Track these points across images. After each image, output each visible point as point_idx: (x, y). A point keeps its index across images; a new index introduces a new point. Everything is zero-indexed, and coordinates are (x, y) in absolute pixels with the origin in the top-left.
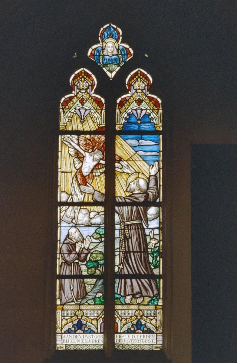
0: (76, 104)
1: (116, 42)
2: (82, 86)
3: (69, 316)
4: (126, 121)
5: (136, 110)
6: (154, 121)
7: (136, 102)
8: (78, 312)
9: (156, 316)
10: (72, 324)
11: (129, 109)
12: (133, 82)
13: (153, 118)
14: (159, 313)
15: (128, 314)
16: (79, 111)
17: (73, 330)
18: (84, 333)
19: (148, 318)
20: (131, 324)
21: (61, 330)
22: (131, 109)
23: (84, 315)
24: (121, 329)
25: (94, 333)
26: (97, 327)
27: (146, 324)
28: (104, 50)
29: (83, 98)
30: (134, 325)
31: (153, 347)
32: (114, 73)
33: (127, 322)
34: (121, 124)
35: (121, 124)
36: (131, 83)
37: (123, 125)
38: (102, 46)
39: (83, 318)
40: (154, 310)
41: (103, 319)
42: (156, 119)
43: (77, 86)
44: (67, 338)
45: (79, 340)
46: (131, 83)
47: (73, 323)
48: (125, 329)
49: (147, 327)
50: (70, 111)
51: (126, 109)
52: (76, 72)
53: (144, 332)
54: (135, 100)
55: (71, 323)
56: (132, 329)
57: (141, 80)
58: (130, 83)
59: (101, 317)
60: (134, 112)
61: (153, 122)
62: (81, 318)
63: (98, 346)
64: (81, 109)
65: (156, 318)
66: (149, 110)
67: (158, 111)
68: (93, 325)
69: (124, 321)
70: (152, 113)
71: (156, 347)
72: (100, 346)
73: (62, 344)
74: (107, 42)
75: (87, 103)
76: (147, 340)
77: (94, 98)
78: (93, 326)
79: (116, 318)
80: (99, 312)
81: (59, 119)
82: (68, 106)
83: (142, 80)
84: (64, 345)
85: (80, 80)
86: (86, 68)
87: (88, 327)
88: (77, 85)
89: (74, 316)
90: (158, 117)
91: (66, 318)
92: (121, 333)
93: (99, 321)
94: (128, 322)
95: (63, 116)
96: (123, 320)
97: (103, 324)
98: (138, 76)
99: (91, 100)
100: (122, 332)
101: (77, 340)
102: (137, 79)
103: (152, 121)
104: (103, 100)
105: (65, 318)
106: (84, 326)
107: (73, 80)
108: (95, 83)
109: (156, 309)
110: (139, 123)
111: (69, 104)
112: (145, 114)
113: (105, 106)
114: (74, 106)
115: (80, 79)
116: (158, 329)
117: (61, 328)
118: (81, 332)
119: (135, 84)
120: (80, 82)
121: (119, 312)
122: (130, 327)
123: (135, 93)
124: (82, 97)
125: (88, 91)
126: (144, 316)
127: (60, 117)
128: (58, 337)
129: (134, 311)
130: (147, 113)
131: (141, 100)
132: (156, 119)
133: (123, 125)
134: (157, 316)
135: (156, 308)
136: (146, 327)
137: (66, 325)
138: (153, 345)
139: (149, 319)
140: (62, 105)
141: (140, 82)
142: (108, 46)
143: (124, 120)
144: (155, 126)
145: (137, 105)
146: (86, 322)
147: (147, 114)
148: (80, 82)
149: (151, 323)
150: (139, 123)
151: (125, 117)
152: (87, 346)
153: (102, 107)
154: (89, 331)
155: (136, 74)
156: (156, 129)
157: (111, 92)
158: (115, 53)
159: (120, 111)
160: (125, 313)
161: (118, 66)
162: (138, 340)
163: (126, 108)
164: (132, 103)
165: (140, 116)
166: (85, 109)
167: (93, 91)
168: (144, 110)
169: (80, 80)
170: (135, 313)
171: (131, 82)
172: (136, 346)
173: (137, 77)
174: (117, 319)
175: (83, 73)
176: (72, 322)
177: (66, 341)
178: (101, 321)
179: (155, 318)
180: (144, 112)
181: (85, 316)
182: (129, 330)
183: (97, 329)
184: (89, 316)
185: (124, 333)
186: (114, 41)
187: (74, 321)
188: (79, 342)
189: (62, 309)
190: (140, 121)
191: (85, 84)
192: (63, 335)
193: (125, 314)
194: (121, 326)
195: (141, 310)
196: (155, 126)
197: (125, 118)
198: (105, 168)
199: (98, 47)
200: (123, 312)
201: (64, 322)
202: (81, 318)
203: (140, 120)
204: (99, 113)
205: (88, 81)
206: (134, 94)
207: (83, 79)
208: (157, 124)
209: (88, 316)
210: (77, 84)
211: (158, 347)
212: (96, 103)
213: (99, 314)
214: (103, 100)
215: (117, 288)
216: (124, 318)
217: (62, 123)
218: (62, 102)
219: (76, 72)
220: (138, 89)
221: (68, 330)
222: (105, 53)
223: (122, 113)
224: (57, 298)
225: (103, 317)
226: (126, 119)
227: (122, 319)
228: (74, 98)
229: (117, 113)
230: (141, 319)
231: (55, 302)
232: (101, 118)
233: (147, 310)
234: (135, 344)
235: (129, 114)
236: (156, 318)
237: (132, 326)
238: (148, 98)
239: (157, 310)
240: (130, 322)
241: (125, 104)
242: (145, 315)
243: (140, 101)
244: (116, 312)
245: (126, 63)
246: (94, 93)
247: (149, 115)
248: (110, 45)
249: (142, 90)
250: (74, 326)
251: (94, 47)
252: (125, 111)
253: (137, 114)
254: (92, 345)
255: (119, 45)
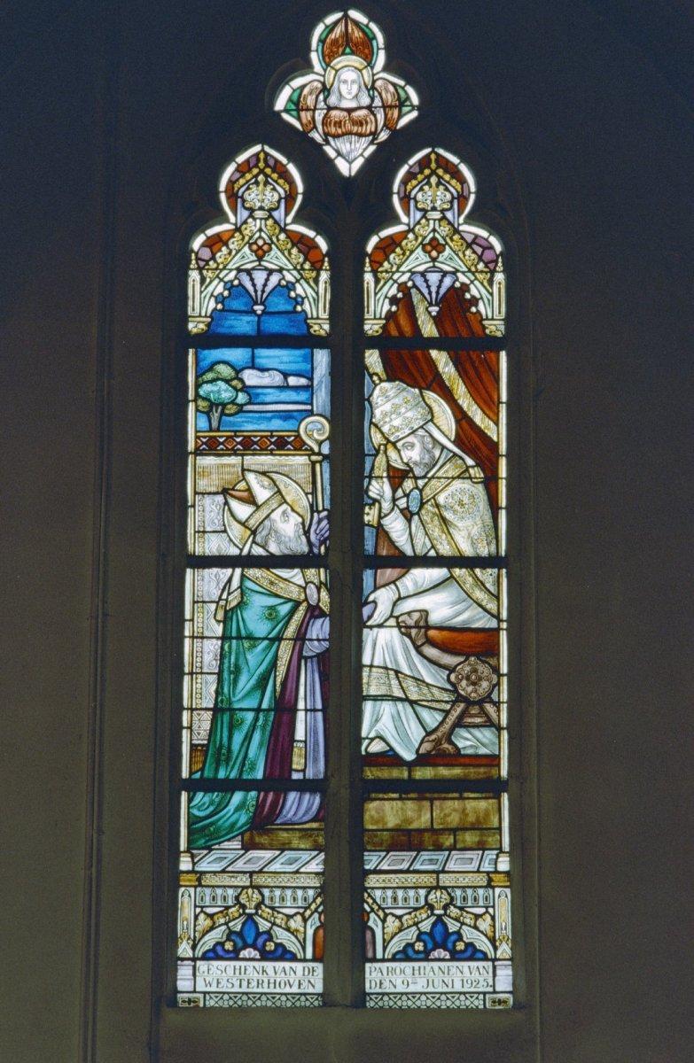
0: (239, 255)
1: (366, 67)
2: (432, 201)
3: (220, 906)
4: (220, 306)
5: (423, 274)
6: (307, 306)
7: (424, 250)
8: (247, 893)
9: (492, 904)
10: (418, 932)
11: (404, 273)
12: (245, 184)
13: (303, 299)
14: (499, 896)
15: (295, 899)
16: (248, 278)
17: (421, 948)
18: (453, 959)
19: (468, 912)
20: (227, 931)
21: (194, 948)
22: (410, 271)
23: (262, 902)
24: (385, 948)
25: (294, 958)
26: (305, 939)
27: (462, 931)
28: (329, 91)
29: (434, 239)
30: (425, 933)
31: (484, 1000)
32: (359, 163)
33: (214, 923)
34: (203, 314)
35: (203, 314)
36: (236, 189)
37: (209, 320)
38: (322, 79)
39: (260, 912)
40: (486, 887)
41: (322, 917)
42: (487, 305)
43: (416, 202)
44: (432, 973)
45: (312, 982)
46: (236, 189)
47: (418, 929)
48: (396, 946)
49: (467, 941)
50: (395, 277)
51: (221, 270)
52: (241, 158)
53: (265, 956)
54: (421, 243)
55: (414, 928)
56: (229, 946)
57: (267, 179)
58: (233, 188)
59: (316, 910)
60: (419, 281)
61: (303, 311)
62: (442, 912)
63: (448, 999)
64: (430, 272)
65: (491, 910)
66: (463, 273)
67: (492, 276)
68: (480, 934)
69: (392, 924)
70: (298, 281)
71: (494, 1002)
72: (472, 997)
73: (195, 992)
74: (337, 67)
75: (272, 253)
76: (302, 981)
77: (469, 238)
78: (481, 935)
79: (368, 914)
80: (311, 893)
81: (363, 308)
82: (389, 263)
83: (269, 180)
84: (201, 996)
85: (253, 180)
86: (272, 146)
87: (465, 939)
88: (415, 198)
89: (234, 906)
90: (317, 293)
91: (210, 911)
92: (383, 960)
93: (309, 923)
94: (406, 926)
95: (201, 292)
96: (390, 919)
97: (321, 932)
98: (429, 167)
99: (456, 243)
100: (386, 957)
101: (441, 981)
102: (428, 177)
103: (299, 308)
104: (323, 245)
105: (204, 909)
106: (453, 938)
107: (405, 182)
108: (469, 190)
109: (492, 884)
110: (259, 312)
111: (392, 256)
112: (279, 284)
113: (503, 262)
114: (233, 261)
115: (424, 179)
116: (497, 944)
117: (194, 940)
118: (256, 955)
119: (247, 192)
120: (426, 188)
121: (378, 894)
122: (274, 939)
123: (250, 220)
124: (431, 235)
125: (277, 214)
126: (455, 907)
127: (366, 296)
128: (184, 971)
129: (422, 892)
130: (283, 283)
131: (439, 244)
132: (487, 305)
133: (209, 320)
134: (493, 907)
135: (490, 880)
136: (270, 939)
137: (396, 934)
138: (485, 994)
139: (469, 915)
140: (371, 261)
141: (265, 185)
142: (343, 77)
143: (212, 305)
144: (308, 321)
145: (255, 258)
146: (270, 925)
147: (283, 287)
148: (426, 188)
149: (288, 929)
150: (259, 312)
151: (215, 294)
152: (472, 997)
153: (492, 266)
154: (468, 953)
155: (424, 163)
156: (485, 333)
157: (347, 215)
158: (365, 101)
159: (201, 274)
160: (225, 897)
161: (372, 143)
162: (260, 982)
163: (221, 267)
164: (412, 252)
165: (263, 291)
166: (441, 271)
167: (461, 220)
168: (450, 272)
169: (253, 180)
170: (426, 897)
171: (409, 187)
172: (293, 998)
173: (427, 172)
174: (372, 915)
175: (262, 161)
176: (416, 924)
177: (208, 980)
178: (314, 922)
179: (487, 912)
180: (274, 279)
181: (266, 906)
182: (410, 952)
183: (304, 948)
184: (279, 907)
185: (394, 959)
186: (356, 61)
187: (234, 920)
188: (313, 986)
189: (197, 883)
190: (262, 307)
191: (442, 197)
192: (198, 963)
193: (225, 900)
194: (384, 940)
195: (445, 888)
196: (308, 321)
197: (216, 298)
198: (186, 450)
199: (310, 82)
200: (389, 893)
201: (203, 922)
202: (253, 911)
203: (262, 303)
204: (308, 283)
205: (450, 184)
206: (419, 223)
207: (261, 178)
208: (490, 317)
209: (277, 905)
210: (245, 191)
211: (500, 1002)
212: (300, 251)
213: (311, 900)
214: (323, 245)
215: (497, 817)
216: (393, 915)
217: (373, 317)
218: (370, 248)
219: (241, 158)
220: (257, 208)
221: (404, 951)
222: (333, 100)
223: (382, 282)
224: (182, 849)
225: (320, 909)
226: (220, 299)
227: (386, 915)
228: (406, 238)
229: (368, 283)
230: (257, 913)
231: (176, 862)
232: (490, 298)
233: (384, 888)
234: (428, 993)
235: (230, 286)
236: (491, 910)
237: (419, 939)
238: (288, 237)
239: (493, 888)
240: (411, 926)
241: (216, 253)
242: (459, 904)
243: (440, 245)
244: (369, 895)
245: (395, 133)
246: (294, 221)
247: (290, 286)
248: (349, 75)
249: (443, 211)
250: (233, 937)
251: (298, 82)
252: (218, 276)
253: (428, 287)
254: (467, 995)
255: (375, 77)
